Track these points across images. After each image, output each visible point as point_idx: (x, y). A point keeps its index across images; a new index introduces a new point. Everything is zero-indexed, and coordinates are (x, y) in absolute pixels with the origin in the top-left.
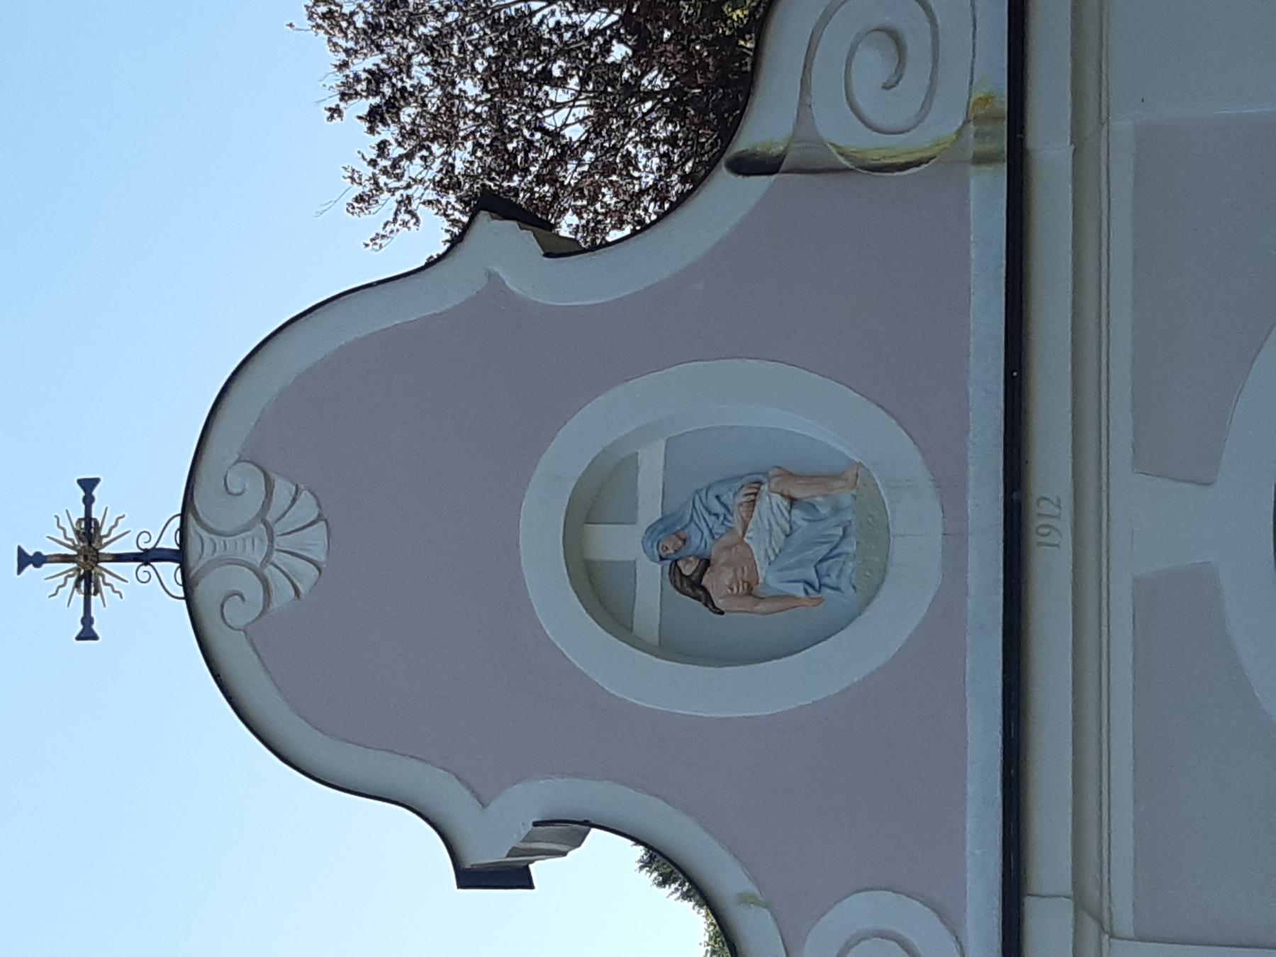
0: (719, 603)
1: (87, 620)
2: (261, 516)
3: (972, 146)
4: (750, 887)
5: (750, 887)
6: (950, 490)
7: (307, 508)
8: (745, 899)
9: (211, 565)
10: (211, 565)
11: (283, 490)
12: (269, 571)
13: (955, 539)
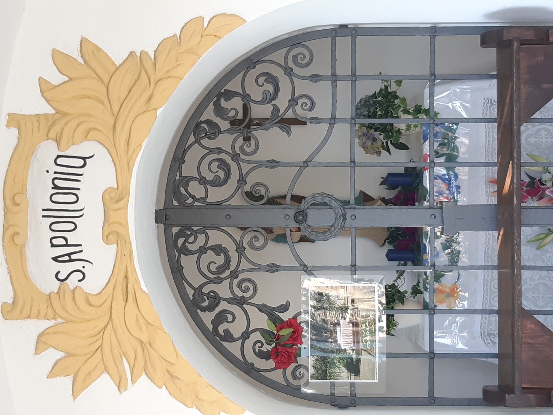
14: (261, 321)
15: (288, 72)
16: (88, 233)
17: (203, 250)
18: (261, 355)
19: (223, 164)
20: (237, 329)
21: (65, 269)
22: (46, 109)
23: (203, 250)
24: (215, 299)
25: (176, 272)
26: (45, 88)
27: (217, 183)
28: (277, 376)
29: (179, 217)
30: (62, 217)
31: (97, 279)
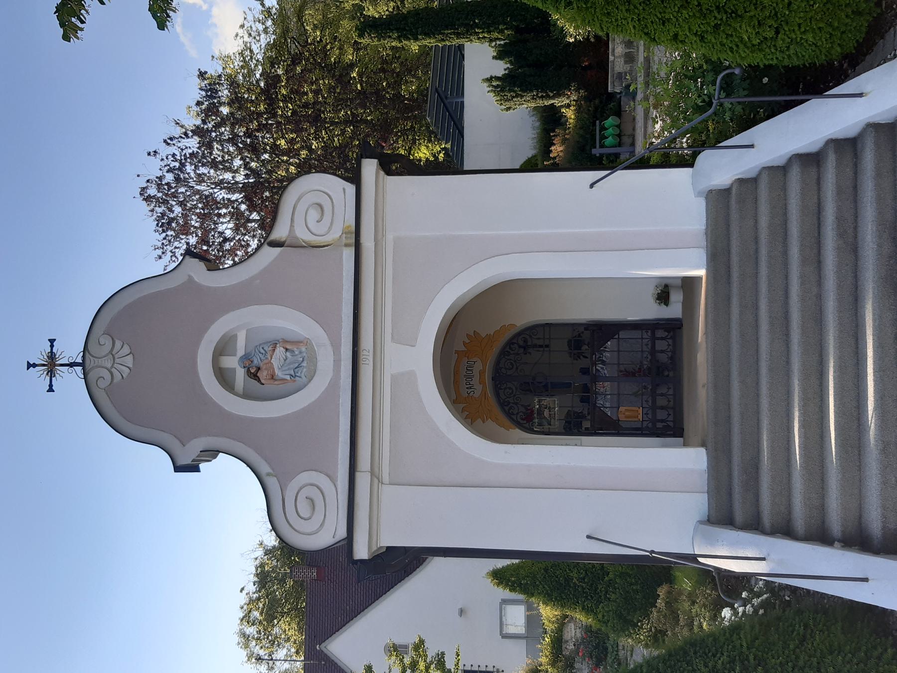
0: (263, 381)
1: (51, 386)
2: (111, 352)
3: (344, 241)
4: (270, 471)
5: (270, 471)
6: (336, 347)
7: (126, 349)
8: (268, 474)
9: (93, 368)
10: (93, 368)
11: (118, 344)
12: (113, 370)
13: (337, 362)
14: (522, 409)
15: (531, 337)
16: (475, 381)
17: (505, 389)
18: (522, 419)
19: (511, 364)
20: (515, 412)
21: (469, 391)
22: (464, 349)
23: (505, 389)
24: (509, 403)
25: (497, 395)
26: (464, 343)
27: (510, 369)
28: (527, 425)
29: (499, 379)
30: (469, 377)
31: (477, 394)
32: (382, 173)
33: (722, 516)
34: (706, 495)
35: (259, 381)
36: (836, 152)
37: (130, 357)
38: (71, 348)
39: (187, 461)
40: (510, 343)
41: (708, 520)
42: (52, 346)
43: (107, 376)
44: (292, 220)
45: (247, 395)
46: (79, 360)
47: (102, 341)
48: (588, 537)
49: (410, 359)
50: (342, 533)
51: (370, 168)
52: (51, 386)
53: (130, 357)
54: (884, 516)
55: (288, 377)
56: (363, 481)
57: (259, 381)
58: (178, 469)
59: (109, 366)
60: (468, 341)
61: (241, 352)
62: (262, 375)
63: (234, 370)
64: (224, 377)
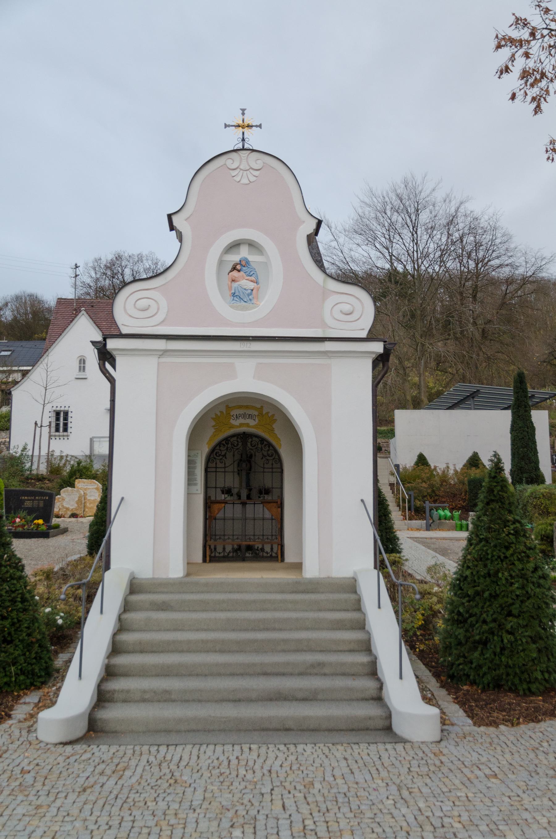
1: (229, 126)
7: (252, 179)
12: (238, 170)
16: (241, 421)
20: (222, 448)
22: (264, 413)
24: (228, 444)
26: (268, 413)
27: (251, 444)
30: (244, 416)
31: (233, 422)
32: (374, 356)
33: (134, 587)
34: (151, 576)
35: (231, 271)
36: (369, 662)
37: (247, 182)
38: (255, 140)
39: (176, 220)
40: (270, 445)
41: (134, 578)
42: (257, 126)
43: (234, 167)
44: (343, 293)
45: (221, 262)
46: (246, 146)
47: (259, 162)
48: (123, 499)
49: (246, 377)
50: (124, 331)
51: (378, 347)
52: (229, 126)
53: (247, 182)
54: (122, 691)
55: (233, 291)
56: (161, 344)
57: (231, 271)
58: (170, 217)
59: (241, 167)
60: (270, 415)
61: (251, 258)
62: (235, 273)
63: (239, 253)
64: (234, 246)
